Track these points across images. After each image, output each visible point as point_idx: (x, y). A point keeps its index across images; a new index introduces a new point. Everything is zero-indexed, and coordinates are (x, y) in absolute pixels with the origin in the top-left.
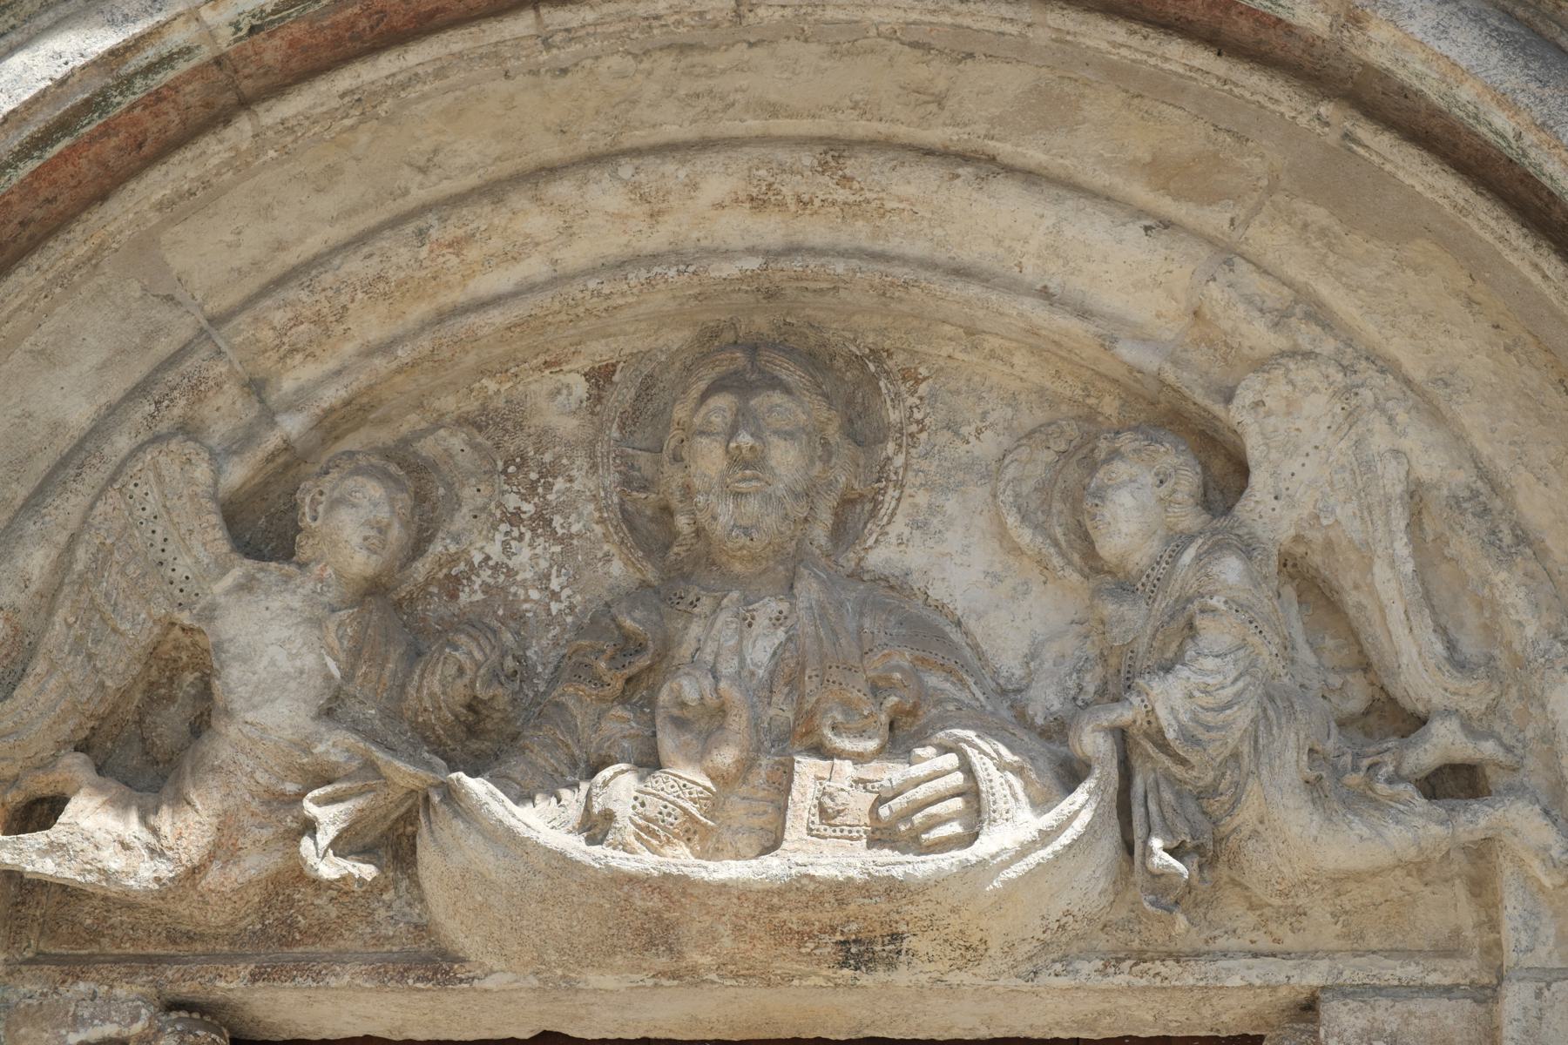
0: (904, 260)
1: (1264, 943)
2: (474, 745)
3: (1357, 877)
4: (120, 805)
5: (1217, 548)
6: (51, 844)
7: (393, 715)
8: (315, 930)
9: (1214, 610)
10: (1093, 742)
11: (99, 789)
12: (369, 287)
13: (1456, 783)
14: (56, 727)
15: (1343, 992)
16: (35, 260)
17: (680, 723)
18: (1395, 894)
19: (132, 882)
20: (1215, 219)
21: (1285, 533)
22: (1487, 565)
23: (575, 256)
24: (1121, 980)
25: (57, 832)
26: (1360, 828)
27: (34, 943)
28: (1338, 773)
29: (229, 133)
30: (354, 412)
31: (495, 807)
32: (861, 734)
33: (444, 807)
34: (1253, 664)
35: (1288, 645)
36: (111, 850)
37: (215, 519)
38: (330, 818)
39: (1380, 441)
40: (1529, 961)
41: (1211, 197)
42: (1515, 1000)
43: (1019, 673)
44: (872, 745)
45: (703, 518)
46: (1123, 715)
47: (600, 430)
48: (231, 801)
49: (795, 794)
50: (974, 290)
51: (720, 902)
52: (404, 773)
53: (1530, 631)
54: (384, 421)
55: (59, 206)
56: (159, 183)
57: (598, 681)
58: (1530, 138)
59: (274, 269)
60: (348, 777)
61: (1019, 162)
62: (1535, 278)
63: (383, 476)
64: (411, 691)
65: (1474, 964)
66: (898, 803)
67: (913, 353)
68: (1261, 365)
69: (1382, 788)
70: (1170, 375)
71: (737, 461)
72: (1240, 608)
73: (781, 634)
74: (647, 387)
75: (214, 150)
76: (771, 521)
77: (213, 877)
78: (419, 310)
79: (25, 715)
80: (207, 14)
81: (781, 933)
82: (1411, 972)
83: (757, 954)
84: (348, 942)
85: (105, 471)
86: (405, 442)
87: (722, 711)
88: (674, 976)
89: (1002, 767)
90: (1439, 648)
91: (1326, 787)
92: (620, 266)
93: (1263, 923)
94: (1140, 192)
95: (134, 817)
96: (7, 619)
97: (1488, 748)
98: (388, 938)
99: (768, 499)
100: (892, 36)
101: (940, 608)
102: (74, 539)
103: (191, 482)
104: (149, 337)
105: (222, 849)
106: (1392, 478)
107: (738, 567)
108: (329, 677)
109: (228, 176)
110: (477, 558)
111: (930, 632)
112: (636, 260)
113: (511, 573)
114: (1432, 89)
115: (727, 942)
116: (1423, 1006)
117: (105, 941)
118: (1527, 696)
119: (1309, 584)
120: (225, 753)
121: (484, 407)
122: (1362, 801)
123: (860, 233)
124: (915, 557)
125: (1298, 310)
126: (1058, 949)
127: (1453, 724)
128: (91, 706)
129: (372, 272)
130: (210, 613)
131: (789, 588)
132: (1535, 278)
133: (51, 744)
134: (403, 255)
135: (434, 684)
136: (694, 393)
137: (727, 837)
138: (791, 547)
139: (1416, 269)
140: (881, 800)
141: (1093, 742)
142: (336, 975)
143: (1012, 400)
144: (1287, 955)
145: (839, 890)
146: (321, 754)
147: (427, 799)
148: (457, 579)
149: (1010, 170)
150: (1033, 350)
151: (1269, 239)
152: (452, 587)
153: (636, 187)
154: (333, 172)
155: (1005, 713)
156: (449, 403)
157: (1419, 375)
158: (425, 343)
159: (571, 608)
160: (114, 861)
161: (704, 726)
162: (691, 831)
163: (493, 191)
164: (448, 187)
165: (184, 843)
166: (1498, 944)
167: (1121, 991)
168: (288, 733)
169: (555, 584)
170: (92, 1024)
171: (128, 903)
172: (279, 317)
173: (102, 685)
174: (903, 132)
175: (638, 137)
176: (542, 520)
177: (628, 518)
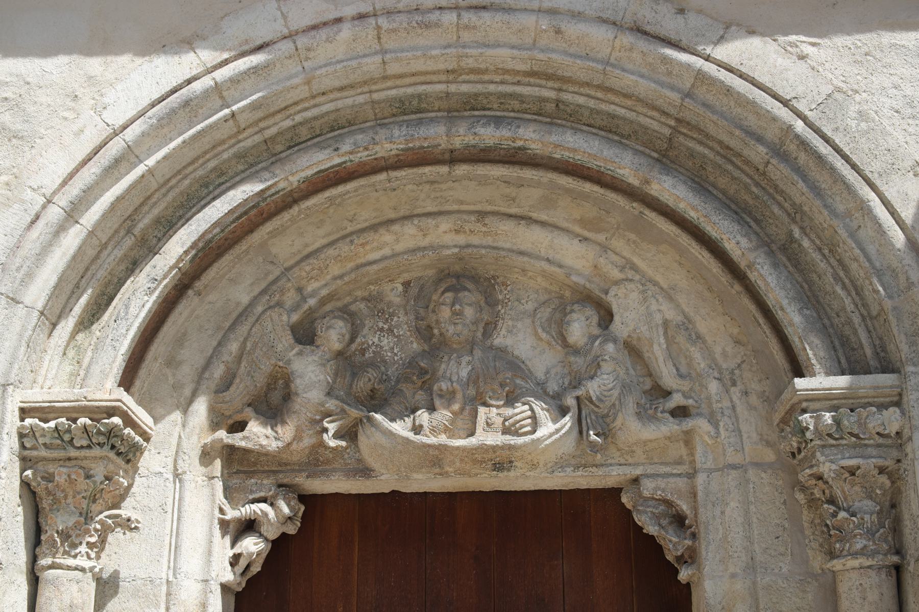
0: (503, 249)
1: (622, 461)
2: (373, 402)
3: (651, 441)
4: (264, 424)
5: (606, 341)
7: (348, 394)
9: (606, 360)
10: (570, 401)
11: (257, 419)
12: (335, 258)
13: (681, 412)
15: (648, 476)
16: (231, 251)
17: (441, 396)
18: (662, 445)
20: (601, 237)
21: (625, 335)
22: (688, 346)
23: (399, 248)
24: (579, 473)
25: (245, 433)
26: (653, 427)
27: (236, 467)
28: (646, 410)
29: (291, 211)
30: (330, 298)
31: (385, 423)
32: (498, 399)
34: (618, 376)
35: (627, 369)
37: (289, 332)
38: (332, 427)
39: (654, 307)
40: (705, 466)
41: (599, 231)
42: (701, 479)
43: (543, 378)
44: (502, 403)
45: (443, 331)
46: (579, 393)
47: (408, 302)
49: (479, 418)
50: (526, 259)
51: (457, 452)
52: (354, 413)
53: (702, 366)
54: (339, 299)
55: (237, 234)
56: (269, 227)
57: (413, 383)
58: (702, 219)
59: (305, 253)
60: (337, 414)
61: (539, 219)
62: (700, 257)
63: (343, 319)
64: (354, 386)
65: (687, 467)
66: (511, 421)
67: (505, 277)
68: (617, 283)
69: (659, 414)
70: (588, 285)
71: (455, 313)
72: (614, 359)
73: (470, 367)
74: (422, 288)
75: (286, 216)
76: (466, 332)
77: (294, 446)
78: (351, 265)
80: (290, 178)
81: (475, 461)
82: (667, 469)
83: (467, 467)
84: (336, 465)
85: (254, 318)
86: (346, 306)
87: (453, 393)
88: (440, 474)
89: (543, 409)
90: (674, 371)
91: (642, 415)
92: (414, 251)
93: (622, 455)
94: (577, 229)
95: (269, 428)
97: (691, 402)
99: (464, 325)
100: (498, 179)
101: (517, 357)
102: (246, 339)
103: (281, 321)
104: (267, 275)
105: (297, 437)
106: (658, 319)
107: (455, 346)
108: (328, 382)
109: (289, 223)
110: (371, 343)
111: (516, 366)
112: (419, 249)
113: (381, 347)
114: (671, 203)
115: (458, 464)
116: (672, 480)
118: (701, 385)
119: (633, 350)
120: (297, 407)
121: (370, 295)
122: (653, 419)
123: (489, 241)
124: (509, 342)
125: (628, 266)
126: (560, 464)
127: (680, 395)
129: (336, 254)
130: (289, 362)
131: (471, 352)
132: (700, 257)
134: (346, 248)
135: (361, 384)
136: (440, 291)
137: (456, 431)
138: (471, 339)
139: (663, 253)
140: (505, 420)
141: (570, 401)
143: (537, 292)
144: (630, 465)
145: (494, 448)
147: (361, 420)
148: (364, 350)
149: (536, 222)
150: (543, 276)
151: (618, 244)
152: (363, 352)
153: (419, 226)
154: (322, 222)
155: (540, 391)
156: (359, 293)
157: (665, 286)
158: (353, 276)
159: (401, 358)
160: (264, 442)
161: (449, 396)
162: (446, 430)
163: (374, 228)
164: (359, 226)
166: (694, 461)
167: (579, 476)
168: (317, 401)
169: (395, 351)
171: (267, 454)
172: (308, 268)
174: (503, 210)
175: (419, 211)
176: (390, 331)
177: (418, 330)
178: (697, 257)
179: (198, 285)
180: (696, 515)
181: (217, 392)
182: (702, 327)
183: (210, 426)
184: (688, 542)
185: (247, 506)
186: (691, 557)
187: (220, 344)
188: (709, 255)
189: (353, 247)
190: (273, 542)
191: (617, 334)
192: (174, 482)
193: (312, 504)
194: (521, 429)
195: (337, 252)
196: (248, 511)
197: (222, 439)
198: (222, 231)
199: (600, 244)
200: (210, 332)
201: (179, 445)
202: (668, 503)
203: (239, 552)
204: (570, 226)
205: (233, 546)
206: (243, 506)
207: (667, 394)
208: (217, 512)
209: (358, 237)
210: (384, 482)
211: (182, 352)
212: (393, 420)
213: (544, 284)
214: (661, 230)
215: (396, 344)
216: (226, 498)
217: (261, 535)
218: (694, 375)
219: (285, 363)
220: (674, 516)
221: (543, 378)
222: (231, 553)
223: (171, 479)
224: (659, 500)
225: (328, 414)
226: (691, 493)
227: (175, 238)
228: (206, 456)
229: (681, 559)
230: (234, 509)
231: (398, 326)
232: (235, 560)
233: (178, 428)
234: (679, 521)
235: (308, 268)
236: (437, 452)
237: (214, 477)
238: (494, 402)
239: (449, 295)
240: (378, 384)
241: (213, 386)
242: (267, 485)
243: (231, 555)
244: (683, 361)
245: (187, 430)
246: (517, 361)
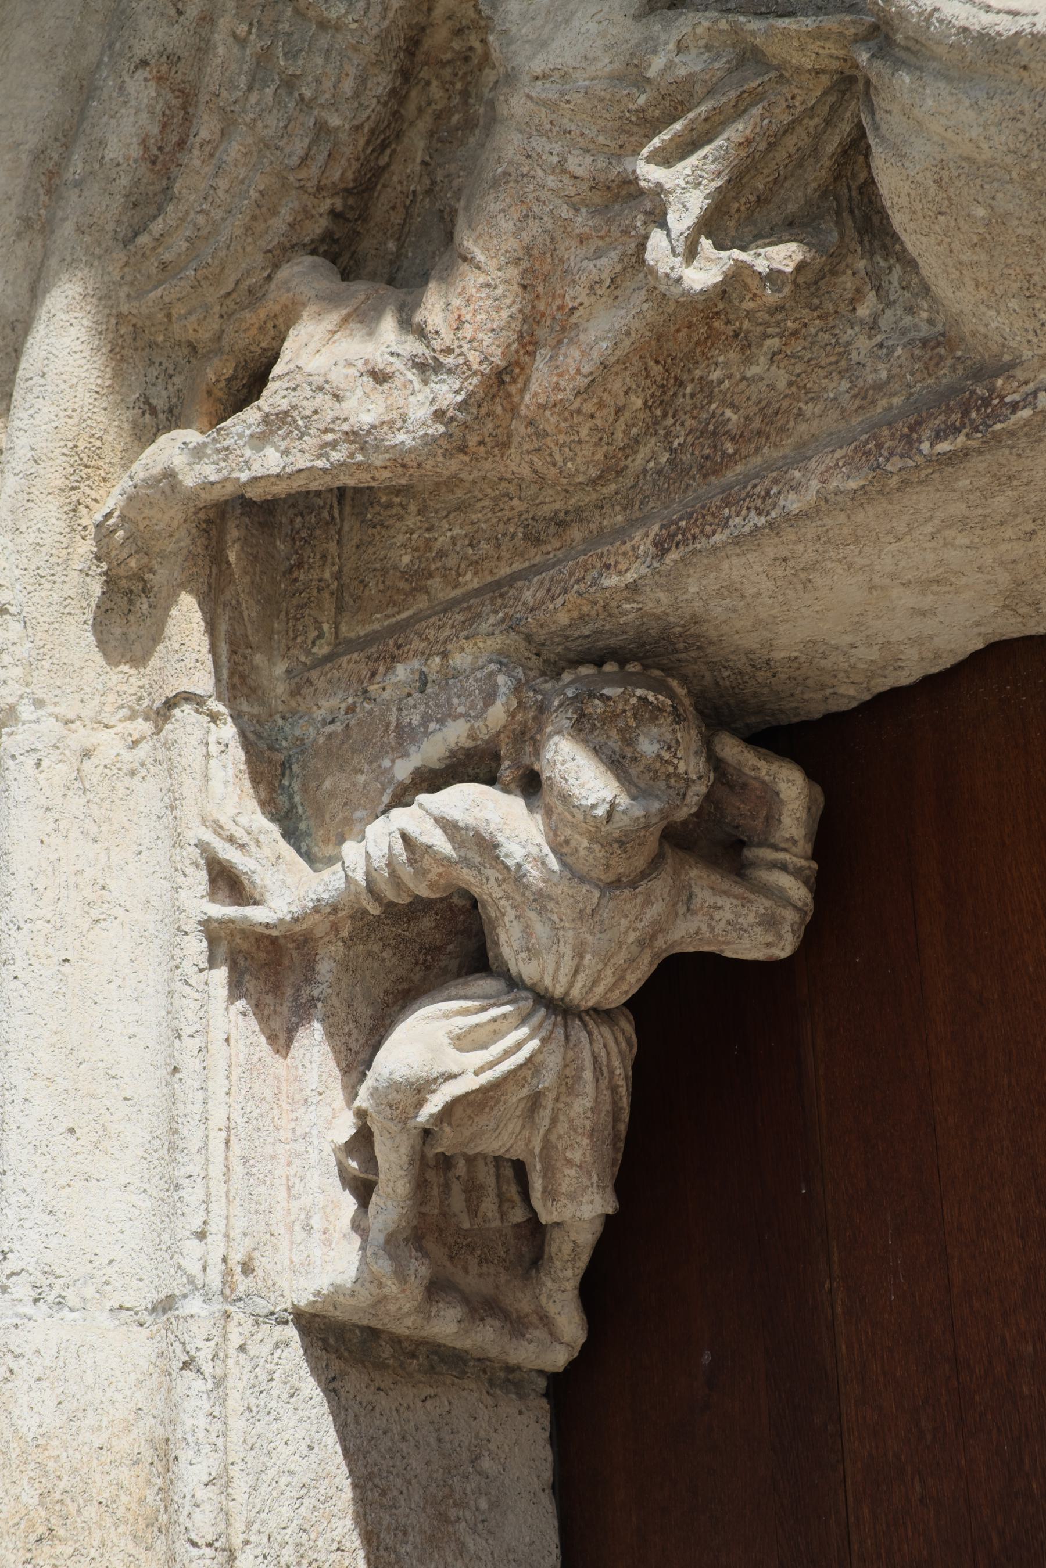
6: (266, 420)
8: (756, 424)
11: (331, 300)
14: (259, 227)
19: (401, 437)
25: (274, 396)
33: (878, 64)
36: (359, 393)
38: (686, 187)
48: (534, 227)
79: (201, 220)
96: (160, 79)
98: (879, 387)
117: (435, 583)
128: (314, 170)
133: (259, 258)
142: (795, 488)
146: (663, 72)
160: (365, 409)
165: (468, 331)
168: (604, 65)
170: (427, 734)
173: (321, 129)
197: (169, 474)
217: (513, 983)
237: (170, 704)
242: (472, 681)
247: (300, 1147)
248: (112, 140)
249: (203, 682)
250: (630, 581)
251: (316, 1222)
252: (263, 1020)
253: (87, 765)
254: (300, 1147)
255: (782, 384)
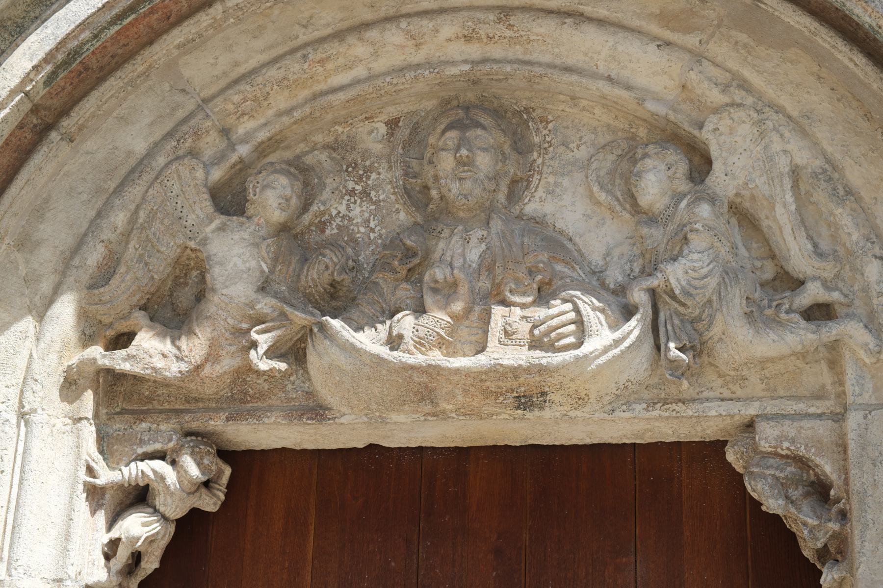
0: (540, 64)
1: (727, 394)
2: (334, 303)
3: (772, 360)
4: (162, 335)
5: (698, 200)
7: (294, 290)
8: (257, 395)
9: (697, 230)
11: (151, 328)
12: (279, 83)
13: (819, 313)
15: (767, 418)
16: (119, 73)
17: (435, 291)
18: (791, 368)
19: (168, 373)
20: (692, 40)
21: (731, 192)
22: (832, 206)
23: (380, 65)
24: (656, 413)
25: (131, 350)
26: (773, 336)
27: (120, 404)
28: (761, 309)
29: (211, 11)
31: (344, 333)
32: (524, 294)
34: (717, 256)
35: (734, 247)
37: (207, 196)
38: (264, 340)
39: (777, 146)
41: (688, 30)
42: (854, 420)
43: (601, 263)
44: (529, 299)
45: (444, 191)
46: (653, 282)
47: (393, 149)
49: (492, 324)
50: (574, 78)
51: (456, 378)
52: (300, 318)
53: (855, 237)
54: (288, 147)
56: (177, 36)
57: (394, 271)
59: (234, 75)
60: (272, 320)
61: (595, 15)
62: (851, 65)
63: (288, 174)
64: (303, 278)
65: (832, 402)
66: (543, 328)
67: (545, 109)
68: (717, 110)
69: (783, 316)
70: (672, 117)
71: (461, 163)
72: (710, 229)
73: (483, 246)
74: (415, 128)
76: (478, 191)
77: (207, 370)
78: (305, 93)
81: (487, 393)
82: (801, 407)
83: (475, 403)
84: (274, 401)
86: (298, 157)
87: (455, 284)
88: (434, 415)
89: (594, 309)
91: (754, 316)
92: (401, 70)
93: (726, 384)
94: (654, 28)
95: (168, 342)
98: (293, 399)
99: (475, 181)
101: (561, 232)
102: (138, 207)
103: (195, 178)
104: (174, 109)
105: (212, 357)
108: (262, 272)
110: (334, 212)
111: (557, 244)
112: (410, 67)
113: (350, 219)
115: (460, 398)
116: (807, 424)
118: (853, 269)
119: (744, 216)
121: (336, 140)
122: (774, 322)
123: (518, 52)
126: (624, 398)
127: (818, 284)
128: (147, 288)
129: (281, 76)
130: (204, 242)
132: (851, 65)
134: (296, 67)
135: (314, 274)
137: (459, 346)
138: (488, 204)
140: (534, 327)
141: (639, 296)
142: (268, 418)
143: (594, 131)
144: (739, 399)
145: (515, 371)
147: (311, 330)
148: (324, 223)
149: (591, 20)
150: (604, 106)
151: (719, 50)
152: (322, 227)
153: (408, 32)
154: (261, 28)
155: (595, 283)
156: (319, 138)
157: (795, 114)
158: (307, 109)
159: (380, 236)
160: (159, 363)
161: (447, 292)
162: (441, 344)
163: (339, 36)
164: (317, 34)
165: (193, 354)
166: (844, 393)
168: (243, 300)
169: (372, 225)
171: (166, 384)
172: (237, 98)
173: (152, 278)
176: (365, 194)
177: (407, 191)
178: (846, 67)
179: (66, 123)
180: (846, 482)
181: (91, 287)
182: (855, 176)
183: (80, 339)
184: (834, 526)
185: (133, 465)
186: (837, 551)
187: (99, 215)
188: (864, 60)
189: (306, 66)
190: (178, 521)
191: (718, 191)
192: (18, 426)
193: (245, 465)
194: (558, 340)
195: (281, 74)
196: (134, 473)
197: (95, 359)
198: (96, 37)
199: (690, 51)
200: (85, 197)
201: (29, 367)
202: (802, 462)
203: (117, 536)
204: (644, 23)
205: (110, 528)
206: (127, 465)
207: (798, 284)
208: (82, 471)
209: (315, 50)
210: (347, 432)
211: (42, 227)
212: (359, 328)
213: (606, 118)
214: (789, 27)
215: (374, 214)
216: (101, 452)
217: (156, 511)
218: (842, 252)
219: (199, 244)
220: (812, 484)
221: (601, 263)
222: (105, 538)
223: (14, 421)
224: (787, 457)
225: (259, 320)
226: (837, 445)
227: (24, 47)
228: (70, 386)
229: (823, 554)
230: (113, 469)
231: (377, 187)
232: (111, 550)
233: (29, 343)
234: (820, 491)
235: (237, 98)
236: (424, 379)
237: (81, 419)
238: (517, 299)
239: (453, 134)
240: (340, 274)
241: (85, 278)
242: (165, 432)
243: (106, 541)
244: (825, 231)
245: (42, 345)
246: (562, 238)
247: (94, 542)
248: (90, 259)
249: (90, 415)
250: (217, 424)
251: (96, 563)
252: (90, 506)
253: (54, 429)
254: (94, 542)
255: (266, 388)
